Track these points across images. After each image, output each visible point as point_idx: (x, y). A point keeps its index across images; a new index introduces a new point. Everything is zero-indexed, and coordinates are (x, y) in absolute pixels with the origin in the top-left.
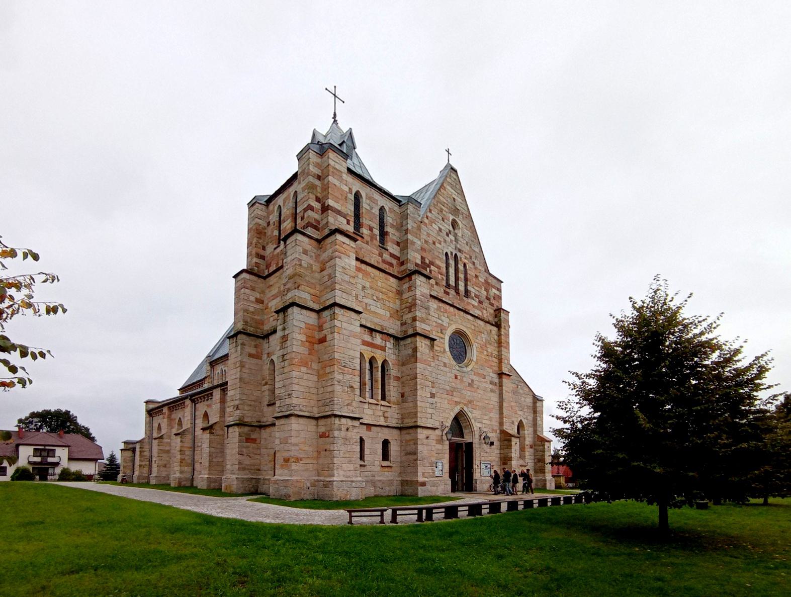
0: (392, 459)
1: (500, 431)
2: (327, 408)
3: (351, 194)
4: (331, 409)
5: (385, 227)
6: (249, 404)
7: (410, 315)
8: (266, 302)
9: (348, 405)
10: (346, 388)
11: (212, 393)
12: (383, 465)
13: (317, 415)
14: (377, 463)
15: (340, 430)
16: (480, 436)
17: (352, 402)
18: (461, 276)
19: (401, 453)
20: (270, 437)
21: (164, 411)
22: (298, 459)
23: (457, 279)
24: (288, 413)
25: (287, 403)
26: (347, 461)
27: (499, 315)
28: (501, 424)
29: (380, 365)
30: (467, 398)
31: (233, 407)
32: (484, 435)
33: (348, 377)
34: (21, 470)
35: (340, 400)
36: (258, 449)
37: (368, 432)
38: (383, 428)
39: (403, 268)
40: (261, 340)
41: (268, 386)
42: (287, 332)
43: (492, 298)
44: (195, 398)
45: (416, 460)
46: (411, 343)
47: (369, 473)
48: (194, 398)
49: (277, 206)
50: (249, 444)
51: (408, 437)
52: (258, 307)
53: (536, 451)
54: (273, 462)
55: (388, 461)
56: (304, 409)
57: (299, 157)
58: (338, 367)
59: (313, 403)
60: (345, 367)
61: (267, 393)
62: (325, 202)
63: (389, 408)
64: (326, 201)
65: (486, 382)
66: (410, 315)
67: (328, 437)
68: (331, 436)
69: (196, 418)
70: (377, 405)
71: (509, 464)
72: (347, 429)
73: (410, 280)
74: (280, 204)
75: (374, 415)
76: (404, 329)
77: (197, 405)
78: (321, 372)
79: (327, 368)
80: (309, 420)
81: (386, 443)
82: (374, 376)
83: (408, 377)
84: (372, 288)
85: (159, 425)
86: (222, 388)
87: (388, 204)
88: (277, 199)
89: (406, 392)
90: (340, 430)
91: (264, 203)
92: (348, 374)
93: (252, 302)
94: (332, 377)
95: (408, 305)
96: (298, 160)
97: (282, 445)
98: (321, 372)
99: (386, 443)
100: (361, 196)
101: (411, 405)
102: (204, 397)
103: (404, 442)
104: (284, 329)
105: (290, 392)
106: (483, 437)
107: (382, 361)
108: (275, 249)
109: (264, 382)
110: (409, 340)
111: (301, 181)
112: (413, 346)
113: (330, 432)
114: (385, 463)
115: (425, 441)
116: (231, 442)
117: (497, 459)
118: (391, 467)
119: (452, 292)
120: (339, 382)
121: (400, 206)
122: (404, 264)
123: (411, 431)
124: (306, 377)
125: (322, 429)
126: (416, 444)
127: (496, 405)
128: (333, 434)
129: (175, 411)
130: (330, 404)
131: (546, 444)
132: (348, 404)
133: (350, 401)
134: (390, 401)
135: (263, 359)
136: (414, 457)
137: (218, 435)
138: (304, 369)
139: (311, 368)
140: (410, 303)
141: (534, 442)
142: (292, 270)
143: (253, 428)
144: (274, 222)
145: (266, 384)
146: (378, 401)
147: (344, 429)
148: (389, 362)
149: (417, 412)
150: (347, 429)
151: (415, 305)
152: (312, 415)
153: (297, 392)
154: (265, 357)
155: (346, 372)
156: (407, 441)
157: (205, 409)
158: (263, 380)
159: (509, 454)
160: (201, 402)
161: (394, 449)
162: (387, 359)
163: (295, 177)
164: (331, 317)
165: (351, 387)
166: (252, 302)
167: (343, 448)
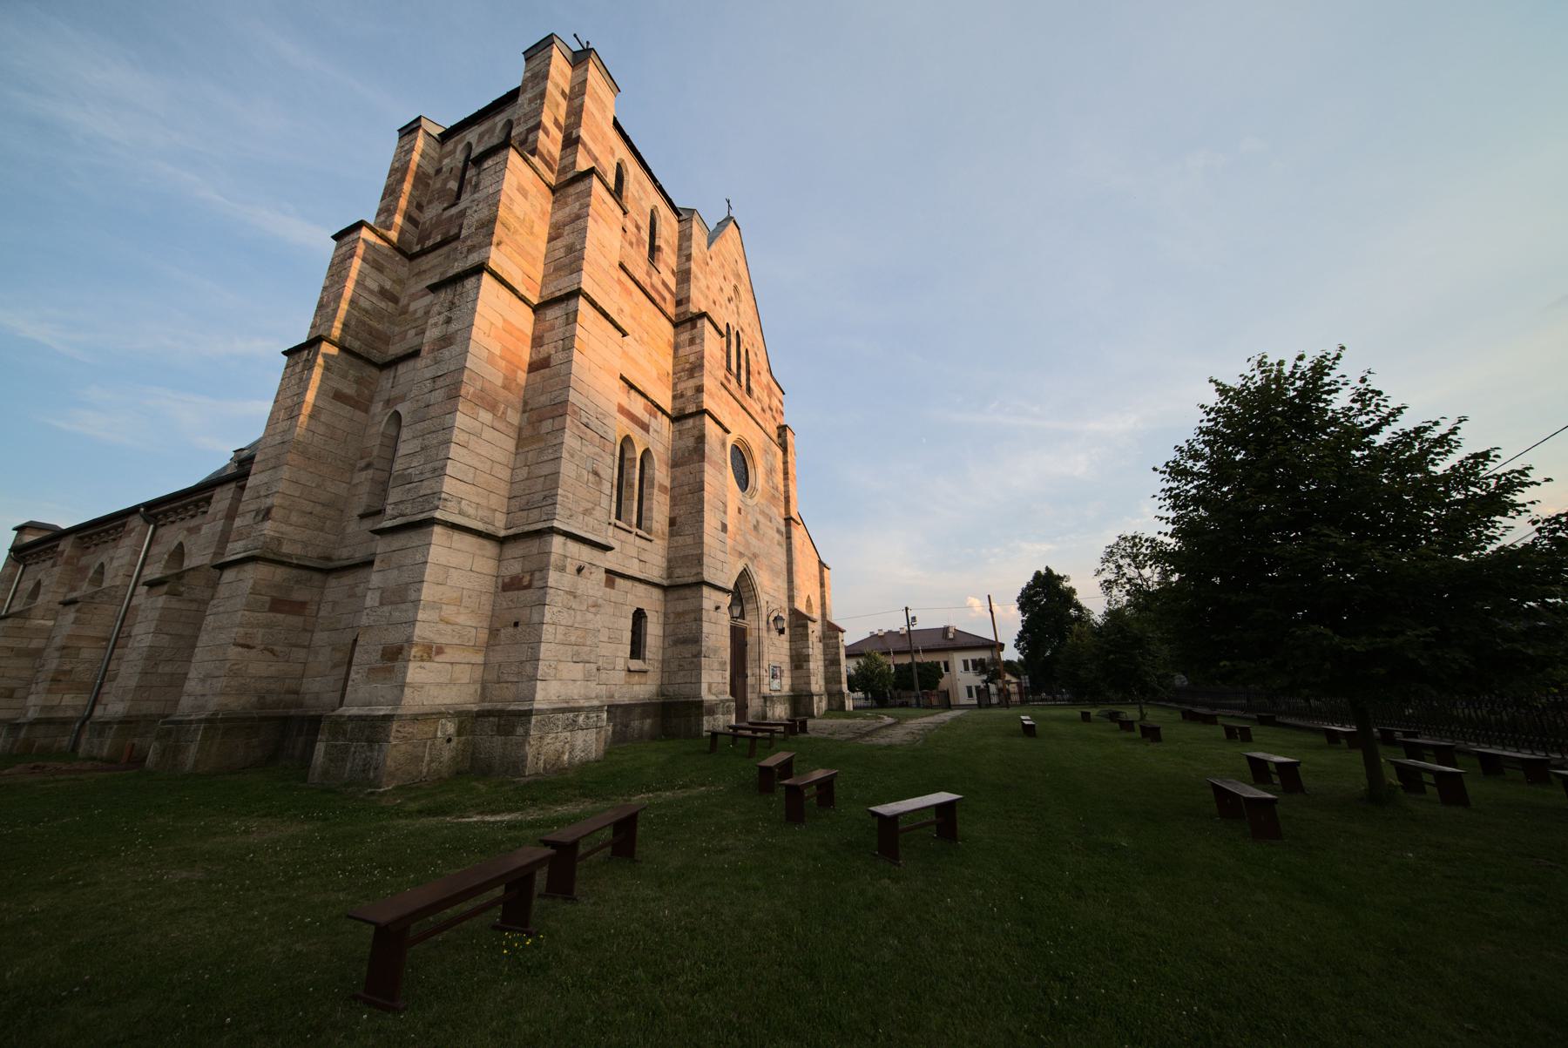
0: (648, 655)
1: (790, 610)
2: (535, 514)
3: (394, 666)
4: (545, 517)
5: (657, 240)
6: (309, 509)
7: (692, 383)
8: (403, 301)
9: (586, 512)
10: (585, 473)
11: (211, 497)
12: (632, 669)
13: (502, 533)
14: (620, 664)
15: (562, 569)
16: (768, 616)
17: (593, 509)
18: (743, 364)
19: (664, 640)
20: (349, 597)
21: (60, 548)
22: (430, 648)
23: (739, 366)
24: (421, 516)
25: (422, 493)
26: (570, 654)
27: (783, 434)
28: (791, 598)
29: (638, 456)
30: (752, 548)
31: (253, 514)
32: (775, 614)
33: (592, 450)
34: (700, 699)
35: (570, 495)
36: (305, 630)
37: (608, 589)
38: (637, 584)
39: (682, 309)
40: (374, 371)
41: (371, 472)
42: (454, 327)
43: (774, 411)
44: (160, 513)
45: (698, 655)
46: (694, 427)
47: (604, 686)
48: (155, 511)
49: (465, 142)
50: (280, 616)
51: (681, 606)
52: (383, 305)
53: (826, 646)
54: (345, 667)
55: (639, 659)
56: (471, 511)
57: (529, 55)
58: (572, 421)
59: (494, 501)
60: (587, 426)
61: (365, 489)
62: (572, 132)
63: (649, 543)
64: (574, 132)
65: (772, 528)
66: (692, 383)
67: (529, 586)
68: (537, 584)
69: (148, 561)
70: (630, 532)
71: (805, 667)
72: (580, 570)
73: (694, 327)
74: (472, 141)
75: (621, 552)
76: (678, 406)
77: (161, 531)
78: (526, 433)
79: (544, 423)
80: (480, 541)
81: (639, 616)
82: (625, 477)
83: (686, 488)
84: (633, 318)
85: (38, 584)
86: (240, 484)
87: (664, 211)
88: (464, 133)
89: (680, 516)
90: (562, 569)
91: (436, 136)
92: (591, 443)
93: (371, 292)
94: (558, 441)
95: (688, 366)
96: (526, 60)
97: (386, 609)
98: (526, 433)
99: (639, 616)
100: (627, 171)
101: (689, 540)
102: (185, 507)
103: (672, 616)
104: (448, 321)
105: (437, 464)
106: (771, 619)
107: (643, 450)
108: (445, 209)
109: (363, 463)
110: (690, 422)
111: (528, 88)
112: (696, 433)
113: (537, 575)
114: (636, 664)
115: (713, 614)
116: (221, 609)
117: (787, 659)
118: (645, 672)
119: (734, 380)
120: (572, 456)
121: (679, 221)
122: (682, 304)
123: (687, 592)
124: (488, 434)
125: (514, 568)
126: (699, 620)
127: (784, 567)
128: (545, 579)
129: (92, 549)
130: (544, 503)
131: (840, 634)
132: (587, 510)
133: (590, 505)
134: (651, 530)
135: (371, 413)
136: (693, 649)
137: (195, 601)
138: (485, 416)
139: (503, 417)
140: (691, 363)
141: (823, 632)
142: (487, 213)
143: (304, 574)
144: (452, 169)
145: (368, 466)
146: (631, 526)
147: (571, 569)
148: (653, 454)
149: (702, 554)
150: (580, 570)
151: (701, 366)
152: (490, 529)
153: (459, 465)
154: (377, 408)
155: (588, 437)
156: (678, 615)
157: (181, 538)
158: (362, 458)
159: (804, 650)
160: (173, 522)
161: (654, 629)
162: (651, 449)
163: (512, 96)
164: (567, 319)
165: (596, 474)
166: (371, 292)
167: (565, 618)
